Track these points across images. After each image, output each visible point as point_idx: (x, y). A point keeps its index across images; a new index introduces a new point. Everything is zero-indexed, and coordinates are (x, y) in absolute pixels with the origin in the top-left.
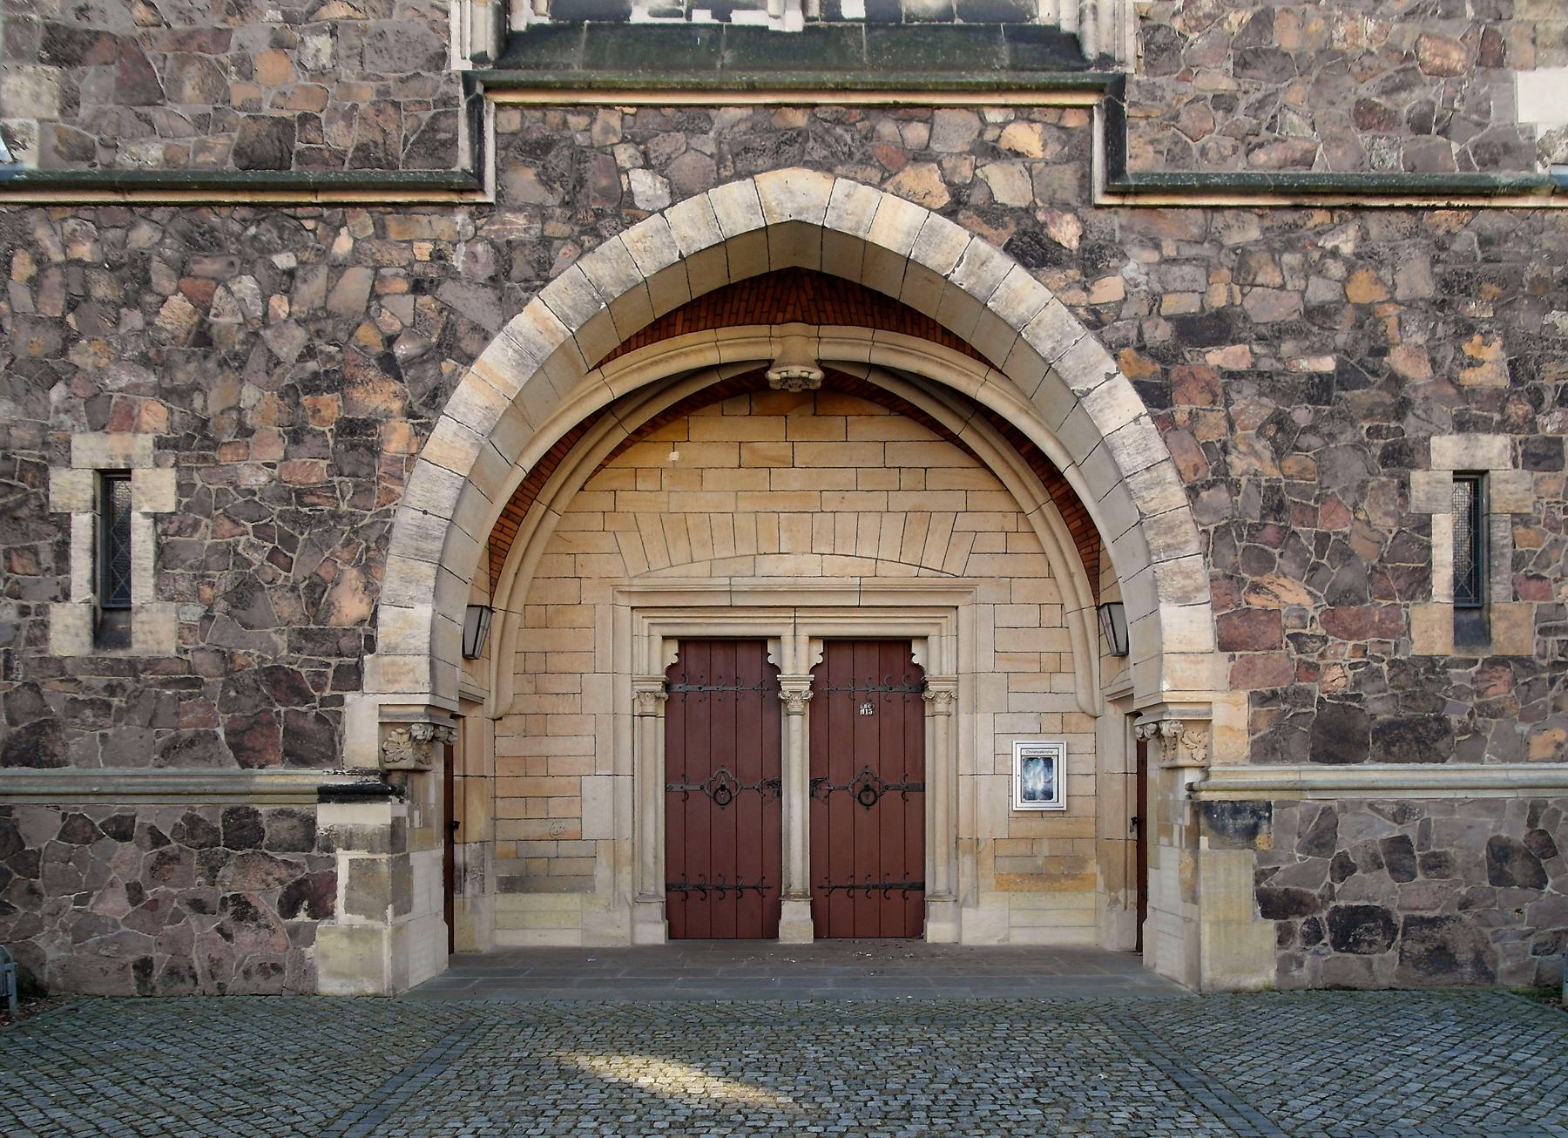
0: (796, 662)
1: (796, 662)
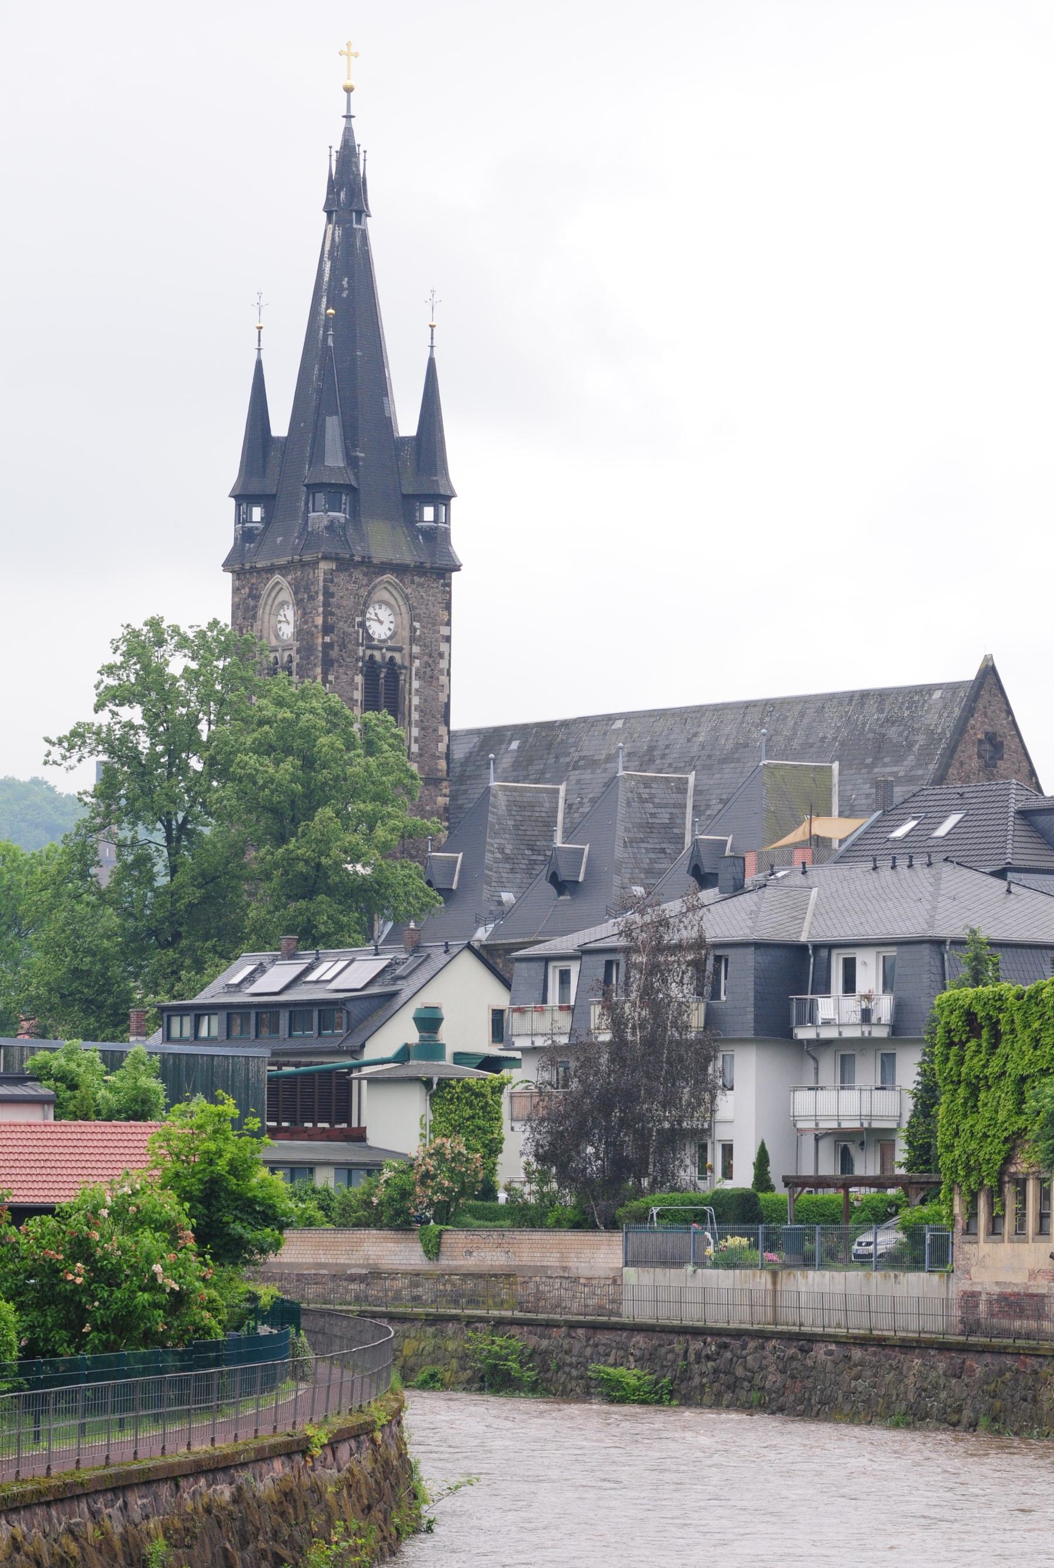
0: (435, 1080)
1: (435, 1080)
